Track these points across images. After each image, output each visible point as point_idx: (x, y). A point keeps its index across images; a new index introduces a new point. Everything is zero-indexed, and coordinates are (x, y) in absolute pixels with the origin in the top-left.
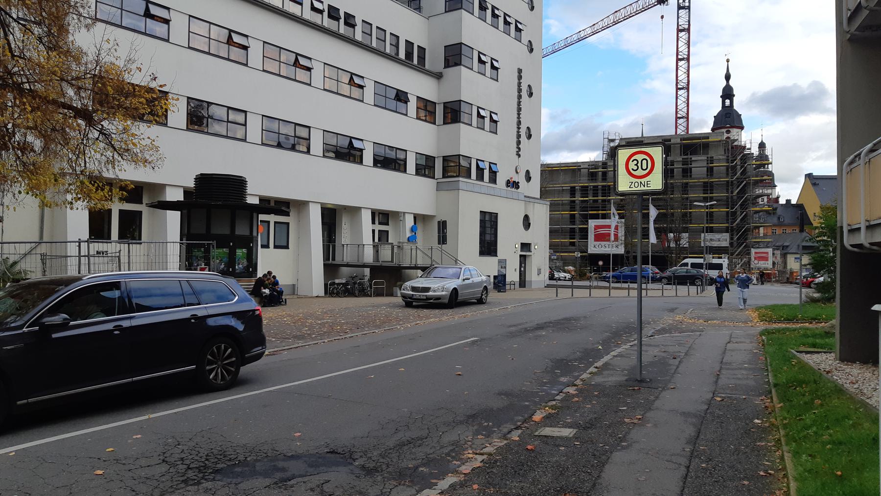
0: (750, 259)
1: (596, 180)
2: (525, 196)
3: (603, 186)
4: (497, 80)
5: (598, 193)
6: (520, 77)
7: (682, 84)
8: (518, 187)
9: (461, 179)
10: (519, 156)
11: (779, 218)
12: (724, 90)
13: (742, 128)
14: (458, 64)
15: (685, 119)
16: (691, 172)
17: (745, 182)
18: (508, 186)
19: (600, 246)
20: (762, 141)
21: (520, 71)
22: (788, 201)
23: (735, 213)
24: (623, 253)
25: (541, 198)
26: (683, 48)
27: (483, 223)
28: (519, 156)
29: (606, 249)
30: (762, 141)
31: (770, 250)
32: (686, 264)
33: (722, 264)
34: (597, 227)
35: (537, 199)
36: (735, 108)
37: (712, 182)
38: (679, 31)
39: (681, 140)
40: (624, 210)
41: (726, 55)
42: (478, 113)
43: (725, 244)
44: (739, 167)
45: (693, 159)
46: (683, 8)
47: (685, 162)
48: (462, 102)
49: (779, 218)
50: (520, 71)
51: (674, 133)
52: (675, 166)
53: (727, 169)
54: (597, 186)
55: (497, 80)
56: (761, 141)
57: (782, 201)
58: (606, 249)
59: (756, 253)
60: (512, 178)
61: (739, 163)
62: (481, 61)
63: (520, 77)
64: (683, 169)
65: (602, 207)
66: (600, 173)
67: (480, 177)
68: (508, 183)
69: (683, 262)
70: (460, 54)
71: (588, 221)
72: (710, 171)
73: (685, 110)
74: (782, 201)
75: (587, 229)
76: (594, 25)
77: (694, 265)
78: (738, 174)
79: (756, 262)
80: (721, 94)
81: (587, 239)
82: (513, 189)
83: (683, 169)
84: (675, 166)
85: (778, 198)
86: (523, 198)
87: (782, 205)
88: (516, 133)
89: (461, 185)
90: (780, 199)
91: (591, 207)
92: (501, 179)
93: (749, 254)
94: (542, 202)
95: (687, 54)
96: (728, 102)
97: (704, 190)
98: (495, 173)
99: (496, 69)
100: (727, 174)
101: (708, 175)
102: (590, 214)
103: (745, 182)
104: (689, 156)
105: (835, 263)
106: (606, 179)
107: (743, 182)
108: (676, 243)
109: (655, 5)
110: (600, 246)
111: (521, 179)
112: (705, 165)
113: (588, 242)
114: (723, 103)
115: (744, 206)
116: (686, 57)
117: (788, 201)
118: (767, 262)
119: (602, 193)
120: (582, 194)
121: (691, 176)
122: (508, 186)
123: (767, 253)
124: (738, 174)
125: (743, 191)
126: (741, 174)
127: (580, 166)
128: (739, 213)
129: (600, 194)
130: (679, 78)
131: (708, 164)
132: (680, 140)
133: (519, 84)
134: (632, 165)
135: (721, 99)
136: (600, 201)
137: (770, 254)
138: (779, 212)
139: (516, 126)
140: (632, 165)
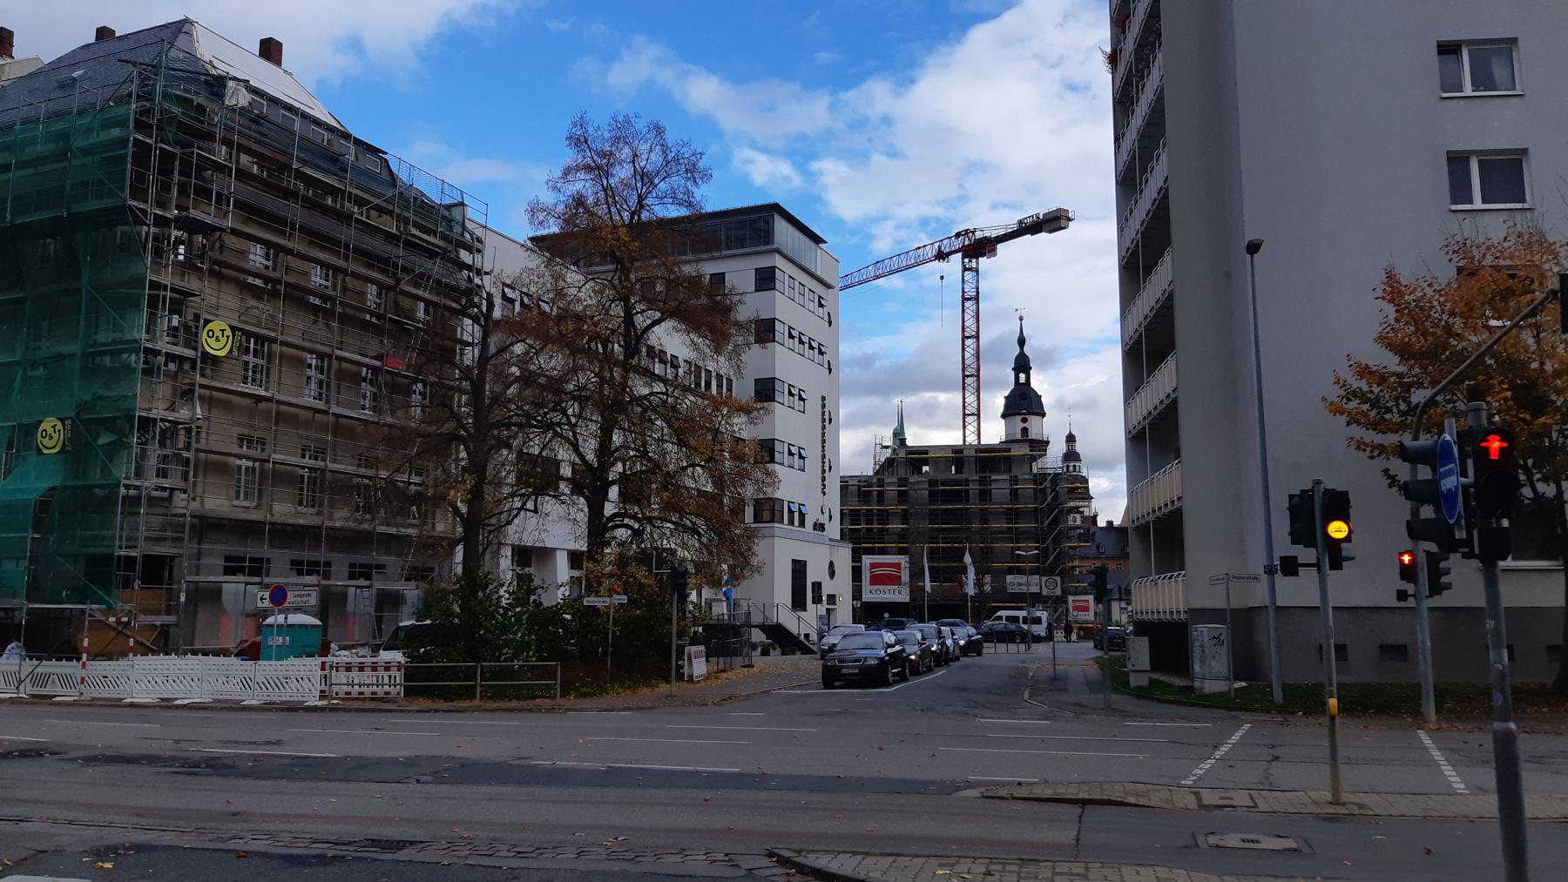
0: (1067, 609)
1: (869, 501)
2: (830, 540)
3: (879, 510)
4: (804, 412)
5: (860, 520)
6: (824, 406)
7: (970, 370)
8: (823, 530)
9: (776, 525)
10: (824, 493)
11: (1098, 548)
12: (1017, 359)
13: (1043, 415)
14: (771, 398)
15: (976, 417)
16: (990, 496)
17: (1057, 510)
18: (815, 529)
19: (878, 592)
20: (1070, 432)
21: (823, 398)
22: (1110, 523)
23: (1047, 548)
24: (908, 601)
25: (842, 539)
26: (970, 322)
27: (794, 571)
28: (824, 493)
29: (885, 596)
30: (1070, 432)
31: (1091, 598)
32: (1000, 618)
33: (1040, 617)
34: (873, 566)
35: (837, 541)
36: (1032, 386)
37: (1018, 508)
38: (964, 300)
39: (976, 453)
40: (907, 543)
41: (1017, 310)
42: (789, 449)
43: (1009, 578)
44: (1049, 490)
45: (993, 478)
46: (970, 269)
47: (983, 482)
48: (776, 441)
49: (1098, 548)
50: (823, 398)
51: (961, 443)
52: (971, 487)
53: (1035, 494)
54: (872, 510)
55: (804, 412)
56: (1068, 432)
57: (1101, 523)
58: (885, 596)
59: (1074, 601)
60: (818, 520)
61: (1049, 486)
62: (791, 394)
63: (824, 406)
64: (980, 491)
65: (880, 539)
66: (875, 493)
67: (791, 522)
68: (815, 524)
69: (997, 615)
70: (774, 389)
71: (861, 558)
72: (1014, 493)
73: (975, 404)
74: (1101, 523)
75: (861, 567)
76: (847, 276)
77: (1009, 618)
78: (1049, 499)
79: (1075, 613)
80: (1013, 366)
81: (861, 582)
82: (819, 533)
83: (980, 491)
84: (971, 487)
85: (1095, 516)
86: (827, 541)
87: (1101, 528)
88: (820, 468)
89: (777, 532)
90: (1098, 518)
91: (865, 538)
92: (809, 522)
93: (1066, 602)
94: (841, 544)
95: (975, 329)
96: (1022, 377)
97: (1007, 519)
98: (804, 515)
99: (803, 400)
100: (1036, 499)
101: (1011, 500)
102: (864, 548)
103: (1057, 510)
104: (988, 474)
105: (601, 694)
106: (883, 501)
107: (1055, 509)
108: (980, 589)
109: (931, 261)
110: (878, 592)
111: (824, 519)
112: (1008, 486)
113: (861, 585)
114: (1017, 378)
115: (1057, 541)
116: (974, 333)
117: (1110, 523)
118: (1087, 613)
119: (878, 520)
120: (851, 520)
121: (990, 500)
122: (815, 529)
123: (1087, 601)
124: (1049, 499)
125: (1055, 522)
126: (1052, 499)
127: (847, 482)
128: (1051, 549)
129: (875, 521)
130: (966, 362)
131: (1011, 485)
132: (974, 451)
133: (823, 413)
134: (1048, 584)
135: (1013, 372)
136: (875, 530)
137: (1092, 603)
138: (1098, 538)
139: (821, 460)
140: (1048, 584)
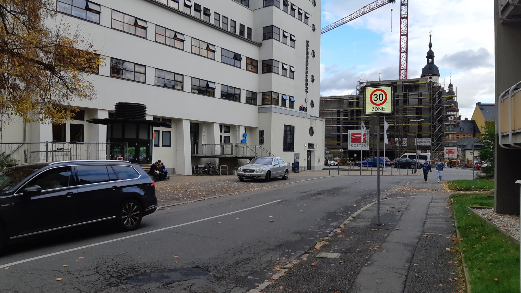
0: (443, 153)
1: (352, 106)
2: (311, 116)
3: (357, 110)
4: (294, 47)
5: (353, 114)
6: (307, 46)
7: (403, 50)
8: (306, 111)
9: (272, 106)
10: (307, 92)
11: (461, 129)
12: (428, 53)
13: (439, 76)
14: (271, 38)
15: (405, 71)
16: (409, 102)
17: (441, 107)
18: (300, 110)
19: (355, 145)
20: (451, 83)
21: (307, 42)
22: (466, 119)
23: (434, 126)
24: (368, 149)
25: (320, 117)
26: (404, 28)
27: (285, 132)
28: (307, 92)
29: (358, 147)
30: (451, 83)
31: (455, 148)
32: (406, 156)
33: (427, 156)
34: (353, 134)
35: (318, 117)
36: (434, 64)
37: (421, 107)
38: (401, 18)
39: (403, 83)
40: (369, 124)
41: (429, 32)
42: (283, 66)
43: (429, 144)
44: (437, 99)
45: (410, 94)
46: (404, 5)
47: (405, 96)
48: (273, 61)
49: (461, 129)
50: (307, 42)
52: (399, 98)
53: (430, 100)
54: (353, 110)
55: (294, 47)
56: (450, 83)
57: (463, 119)
58: (358, 147)
59: (447, 149)
60: (303, 105)
61: (437, 96)
62: (284, 36)
63: (307, 46)
64: (404, 100)
65: (356, 122)
66: (355, 102)
67: (284, 105)
68: (300, 108)
69: (404, 155)
70: (272, 32)
71: (348, 131)
72: (420, 101)
73: (405, 65)
74: (463, 119)
75: (347, 135)
76: (351, 15)
77: (410, 157)
78: (437, 103)
79: (447, 155)
80: (426, 56)
81: (347, 141)
82: (304, 112)
83: (404, 100)
84: (399, 98)
85: (460, 117)
86: (309, 117)
87: (462, 121)
88: (305, 79)
89: (273, 110)
90: (461, 117)
91: (350, 122)
92: (296, 106)
93: (443, 150)
94: (320, 119)
95: (406, 32)
96: (430, 60)
97: (416, 112)
98: (293, 102)
99: (294, 41)
100: (430, 103)
101: (418, 103)
102: (349, 126)
103: (441, 107)
104: (408, 92)
105: (494, 155)
106: (358, 106)
107: (439, 107)
108: (400, 143)
109: (387, 3)
110: (355, 145)
111: (308, 105)
112: (417, 97)
113: (347, 143)
114: (428, 61)
115: (440, 122)
116: (405, 33)
117: (466, 119)
118: (453, 155)
119: (356, 114)
120: (344, 114)
121: (408, 104)
122: (300, 110)
123: (454, 149)
124: (437, 103)
125: (439, 113)
126: (438, 103)
127: (343, 98)
128: (437, 126)
129: (355, 115)
130: (401, 46)
131: (418, 97)
132: (402, 83)
133: (307, 50)
134: (374, 98)
135: (426, 58)
136: (355, 119)
137: (456, 150)
138: (461, 125)
139: (305, 74)
140: (374, 98)
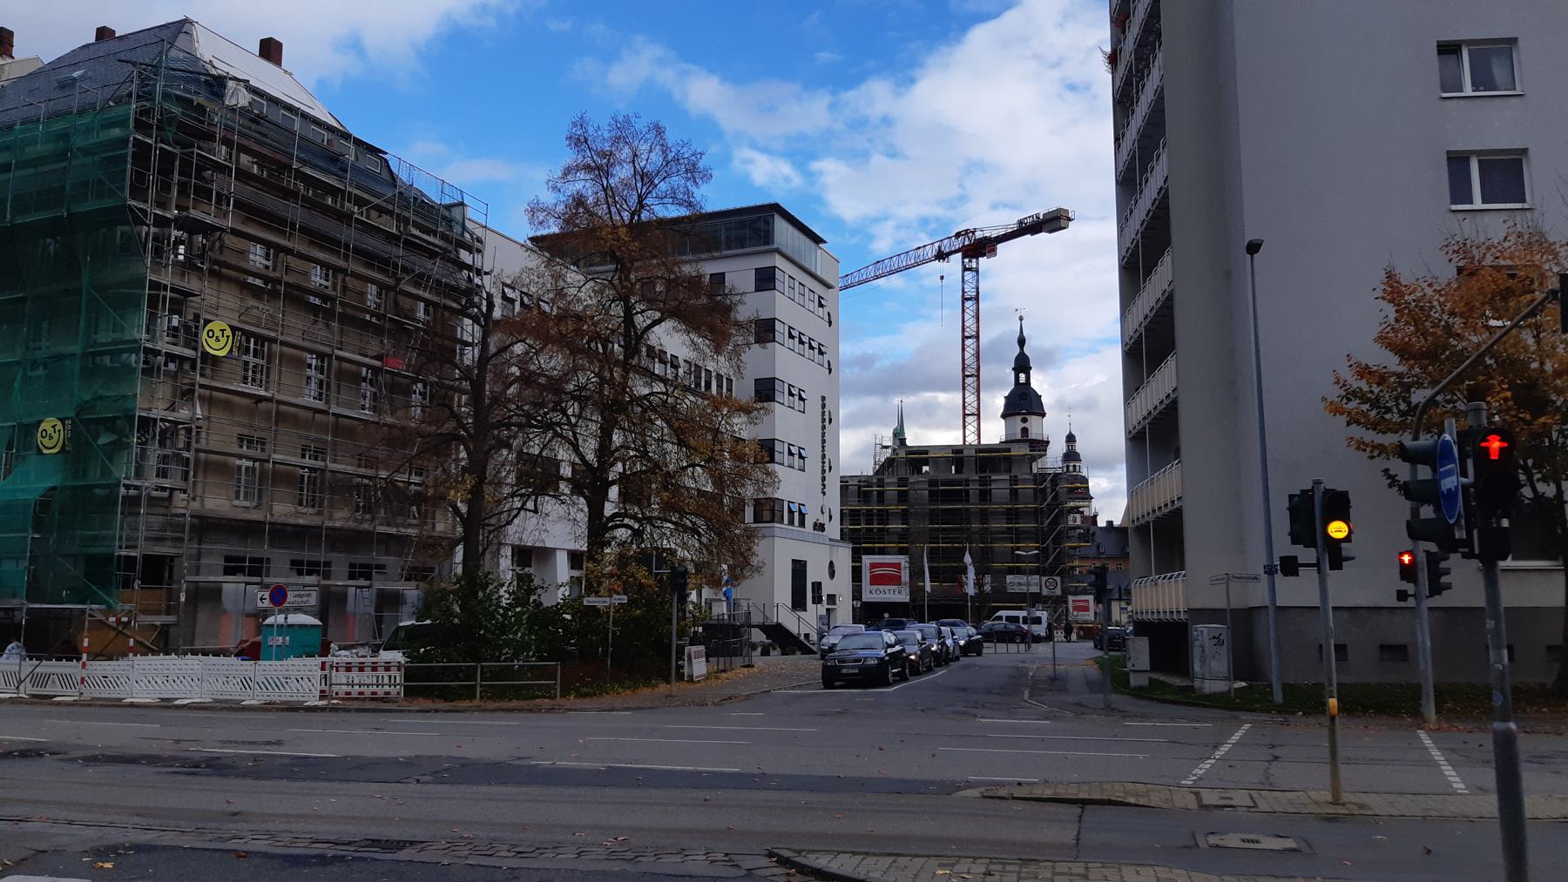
0: (1067, 609)
1: (869, 501)
2: (830, 540)
3: (879, 510)
4: (804, 412)
5: (860, 520)
6: (824, 406)
7: (970, 370)
8: (823, 530)
9: (776, 525)
10: (824, 493)
11: (1098, 548)
12: (1017, 359)
13: (1043, 415)
14: (771, 398)
15: (976, 417)
16: (990, 496)
17: (1057, 510)
18: (815, 529)
19: (878, 592)
20: (1070, 432)
21: (823, 398)
22: (1110, 523)
23: (1047, 548)
24: (908, 601)
25: (842, 539)
26: (970, 322)
27: (794, 571)
28: (824, 493)
29: (885, 596)
30: (1070, 432)
31: (1091, 598)
32: (1000, 618)
33: (1040, 617)
34: (873, 566)
35: (837, 541)
36: (1032, 386)
37: (1018, 508)
38: (964, 300)
39: (976, 453)
40: (907, 543)
41: (1017, 310)
42: (789, 449)
43: (1009, 578)
44: (1049, 490)
45: (993, 478)
46: (970, 269)
47: (983, 482)
48: (776, 441)
49: (1098, 548)
50: (823, 398)
51: (961, 443)
52: (971, 487)
53: (1035, 494)
54: (872, 510)
55: (804, 412)
56: (1068, 432)
57: (1101, 523)
58: (885, 596)
59: (1074, 601)
60: (818, 520)
61: (1049, 486)
62: (791, 394)
63: (824, 406)
64: (980, 491)
65: (880, 539)
66: (875, 493)
67: (791, 522)
68: (815, 524)
69: (997, 615)
70: (774, 389)
71: (861, 558)
72: (1014, 493)
73: (975, 404)
74: (1101, 523)
75: (861, 567)
76: (847, 276)
77: (1009, 618)
78: (1049, 499)
79: (1075, 613)
80: (1013, 366)
81: (861, 582)
82: (819, 533)
83: (980, 491)
84: (971, 487)
85: (1095, 516)
86: (827, 541)
87: (1101, 528)
88: (820, 468)
89: (777, 532)
90: (1098, 518)
91: (865, 538)
92: (809, 522)
93: (1066, 602)
94: (841, 544)
95: (975, 329)
96: (1022, 377)
97: (1007, 519)
98: (804, 515)
99: (803, 400)
100: (1036, 499)
101: (1011, 500)
102: (864, 548)
103: (1057, 510)
104: (988, 474)
105: (601, 694)
106: (883, 501)
107: (1055, 509)
108: (980, 589)
109: (931, 261)
110: (878, 592)
111: (824, 519)
112: (1008, 486)
113: (861, 585)
114: (1017, 378)
115: (1057, 541)
116: (974, 333)
117: (1110, 523)
118: (1087, 613)
119: (878, 520)
120: (851, 520)
121: (990, 500)
122: (815, 529)
123: (1087, 601)
124: (1049, 499)
125: (1055, 522)
126: (1052, 499)
127: (847, 482)
128: (1051, 549)
129: (875, 521)
130: (966, 362)
131: (1011, 485)
132: (974, 451)
133: (823, 413)
134: (1048, 584)
135: (1013, 372)
136: (875, 530)
137: (1092, 603)
138: (1098, 538)
139: (821, 460)
140: (1048, 584)
